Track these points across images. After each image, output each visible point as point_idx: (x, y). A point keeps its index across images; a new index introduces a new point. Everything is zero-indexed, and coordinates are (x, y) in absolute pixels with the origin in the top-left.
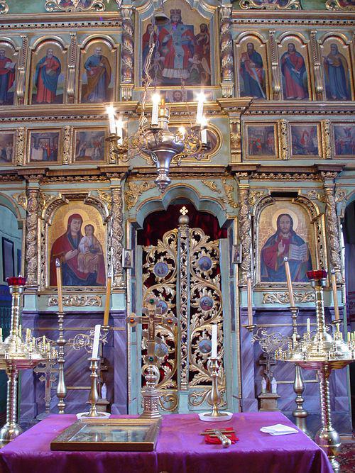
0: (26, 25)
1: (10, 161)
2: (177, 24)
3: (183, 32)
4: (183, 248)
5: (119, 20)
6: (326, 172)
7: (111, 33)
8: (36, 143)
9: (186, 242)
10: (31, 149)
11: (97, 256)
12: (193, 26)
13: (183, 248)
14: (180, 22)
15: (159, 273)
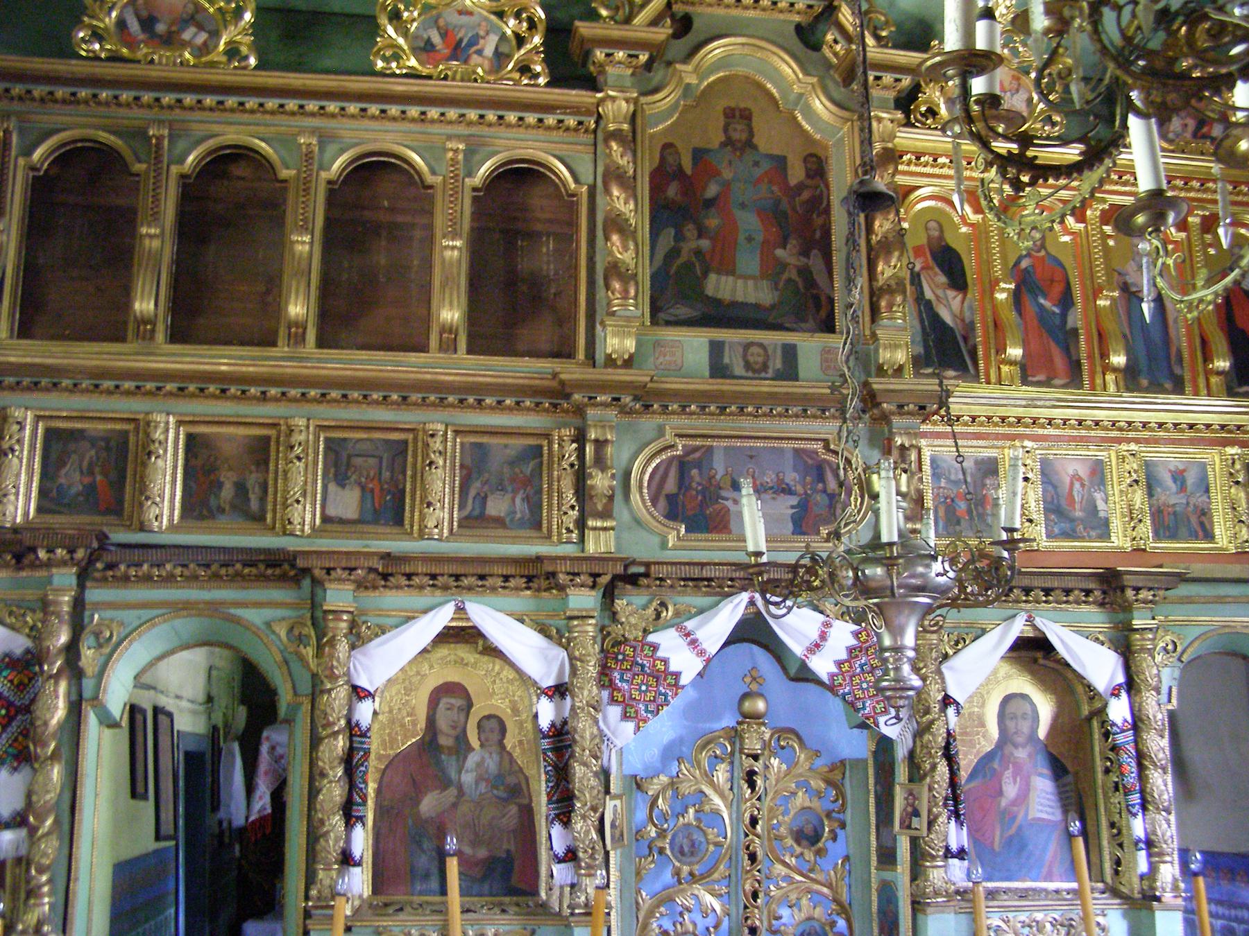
0: (312, 106)
1: (260, 518)
2: (742, 150)
3: (758, 172)
4: (752, 785)
5: (588, 113)
6: (1137, 589)
7: (564, 150)
8: (340, 462)
9: (758, 766)
10: (325, 487)
11: (513, 809)
12: (784, 158)
13: (752, 785)
14: (749, 144)
15: (682, 853)
